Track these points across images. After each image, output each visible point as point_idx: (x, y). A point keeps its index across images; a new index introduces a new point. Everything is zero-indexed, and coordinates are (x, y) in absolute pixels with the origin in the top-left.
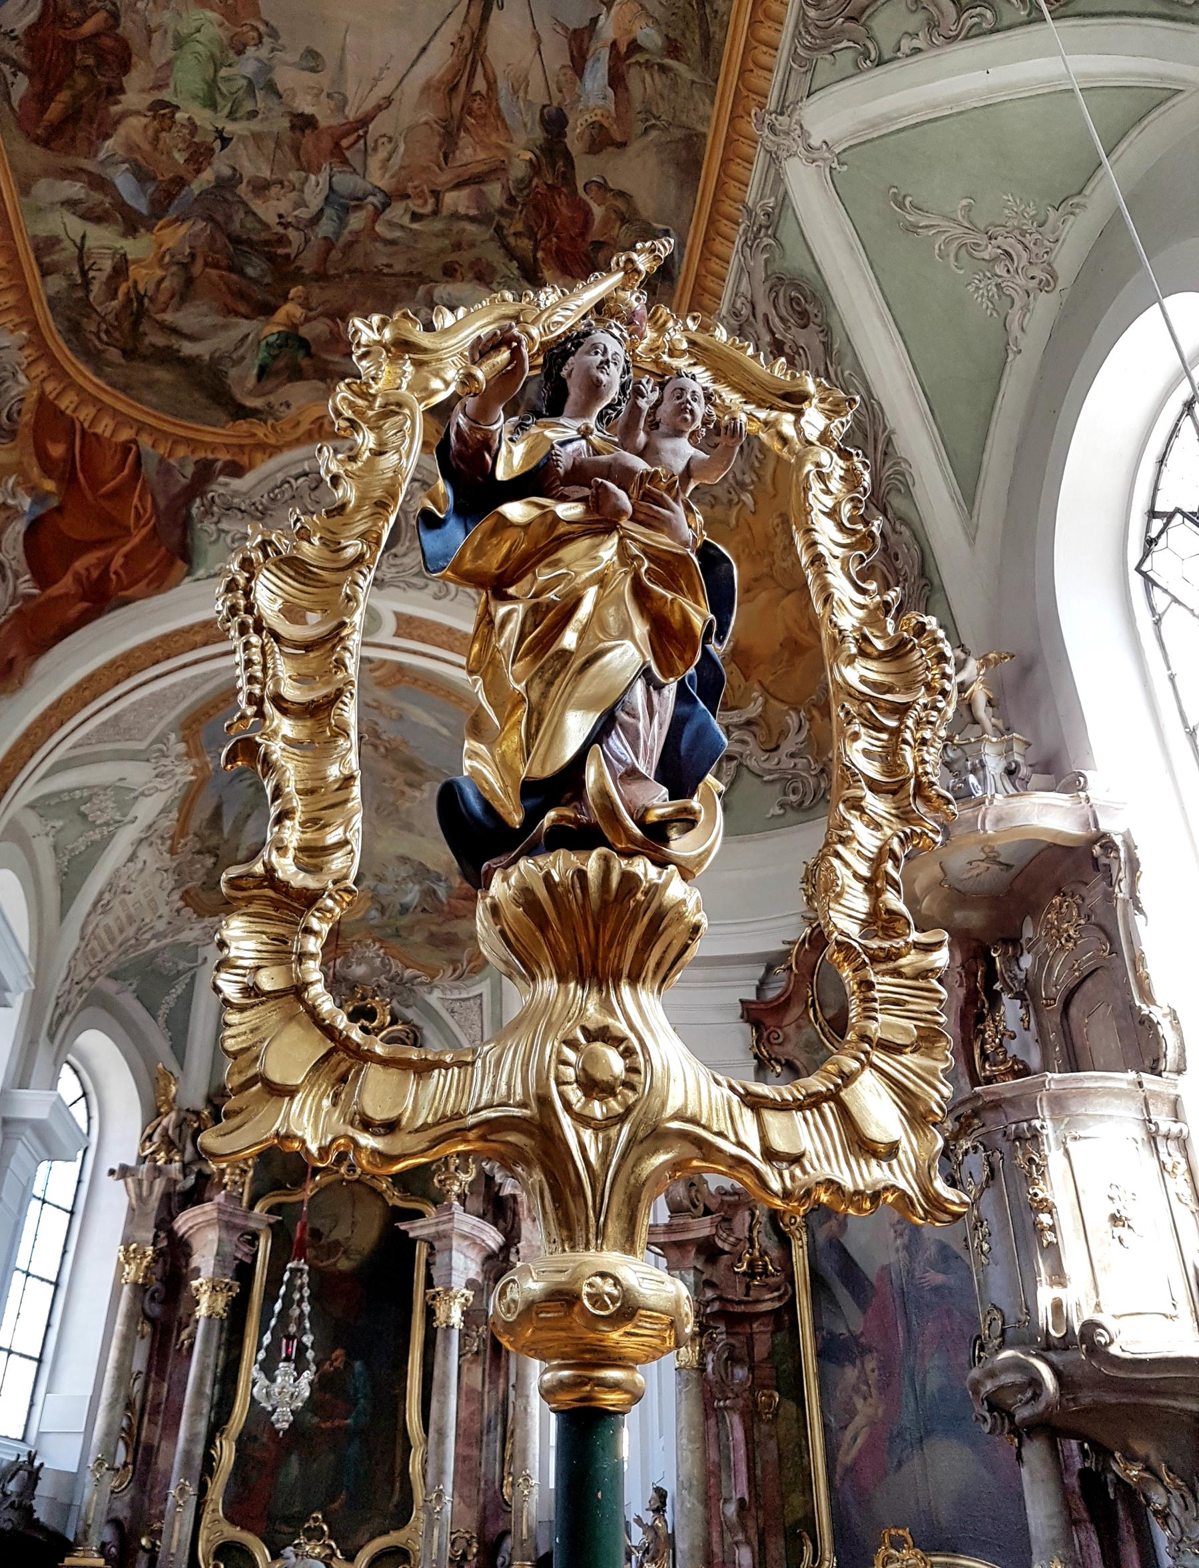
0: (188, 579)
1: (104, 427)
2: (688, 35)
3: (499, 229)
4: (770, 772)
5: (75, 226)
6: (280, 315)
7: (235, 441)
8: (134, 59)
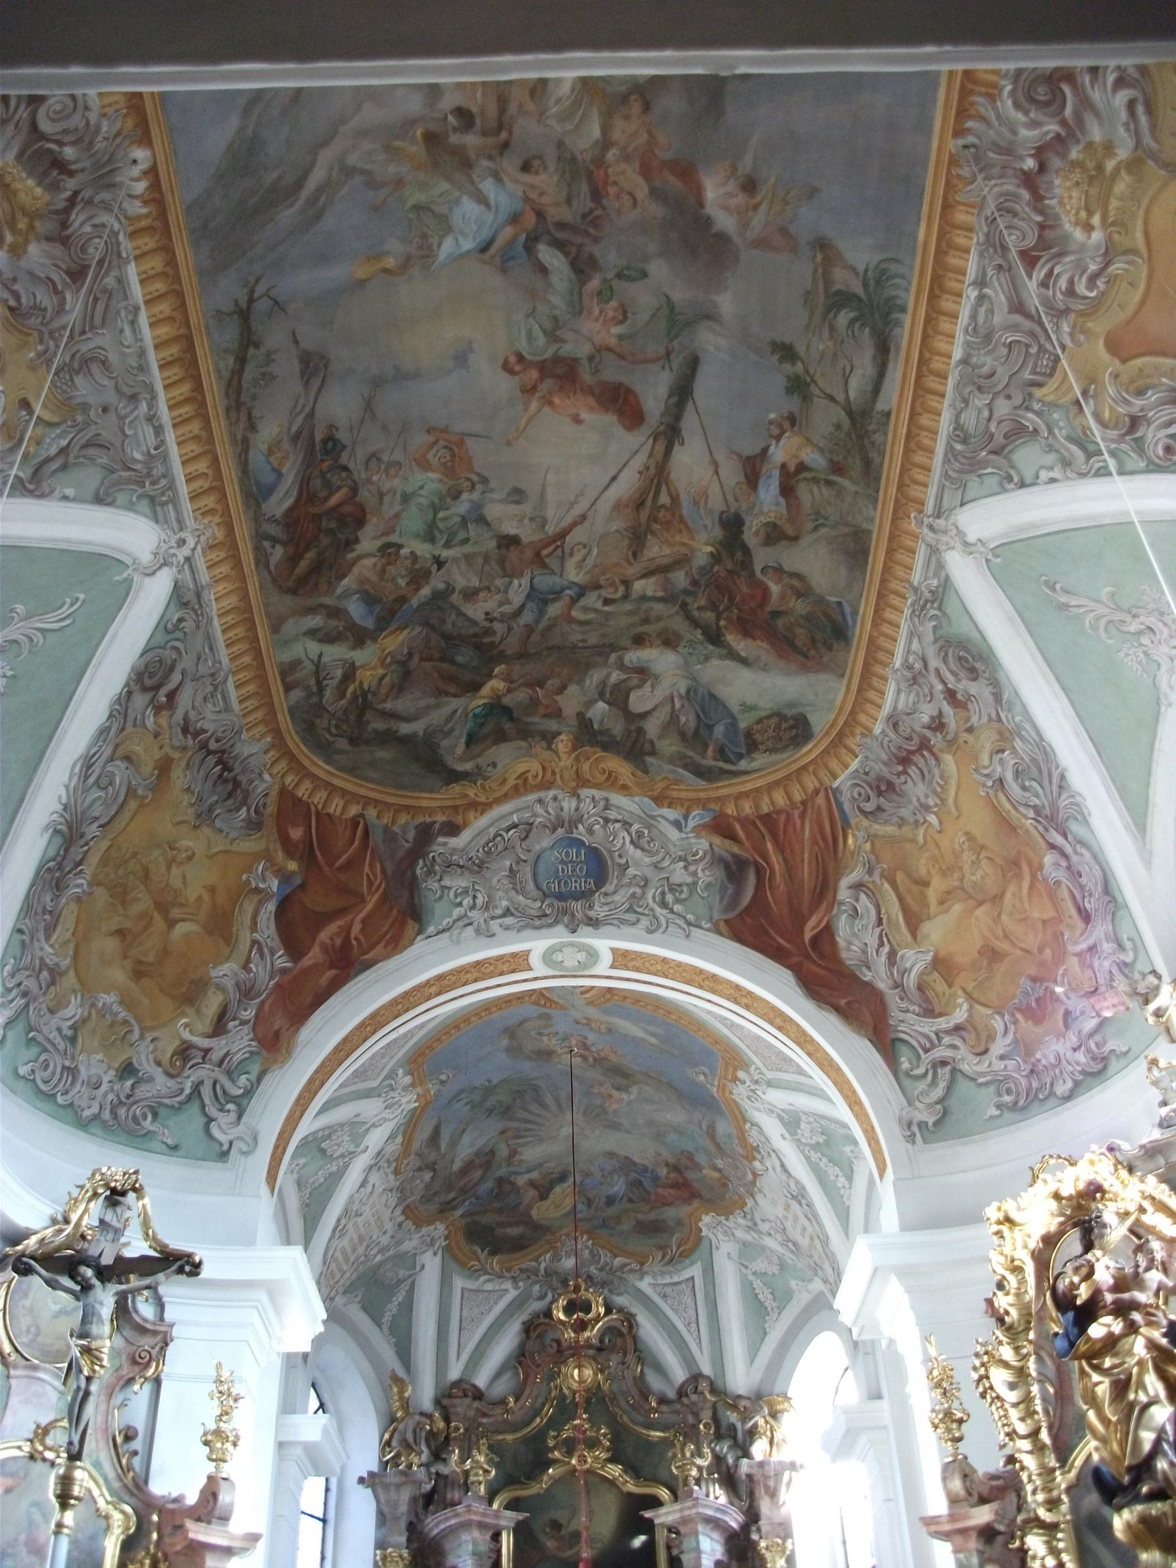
0: (419, 938)
1: (335, 807)
3: (684, 606)
4: (983, 1074)
6: (486, 690)
7: (450, 803)
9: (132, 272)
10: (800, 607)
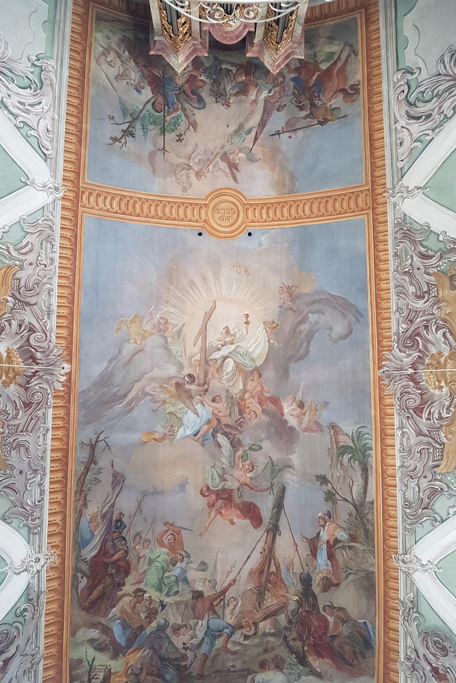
2: (358, 531)
3: (285, 638)
5: (91, 652)
8: (131, 570)
9: (50, 412)
10: (345, 630)
